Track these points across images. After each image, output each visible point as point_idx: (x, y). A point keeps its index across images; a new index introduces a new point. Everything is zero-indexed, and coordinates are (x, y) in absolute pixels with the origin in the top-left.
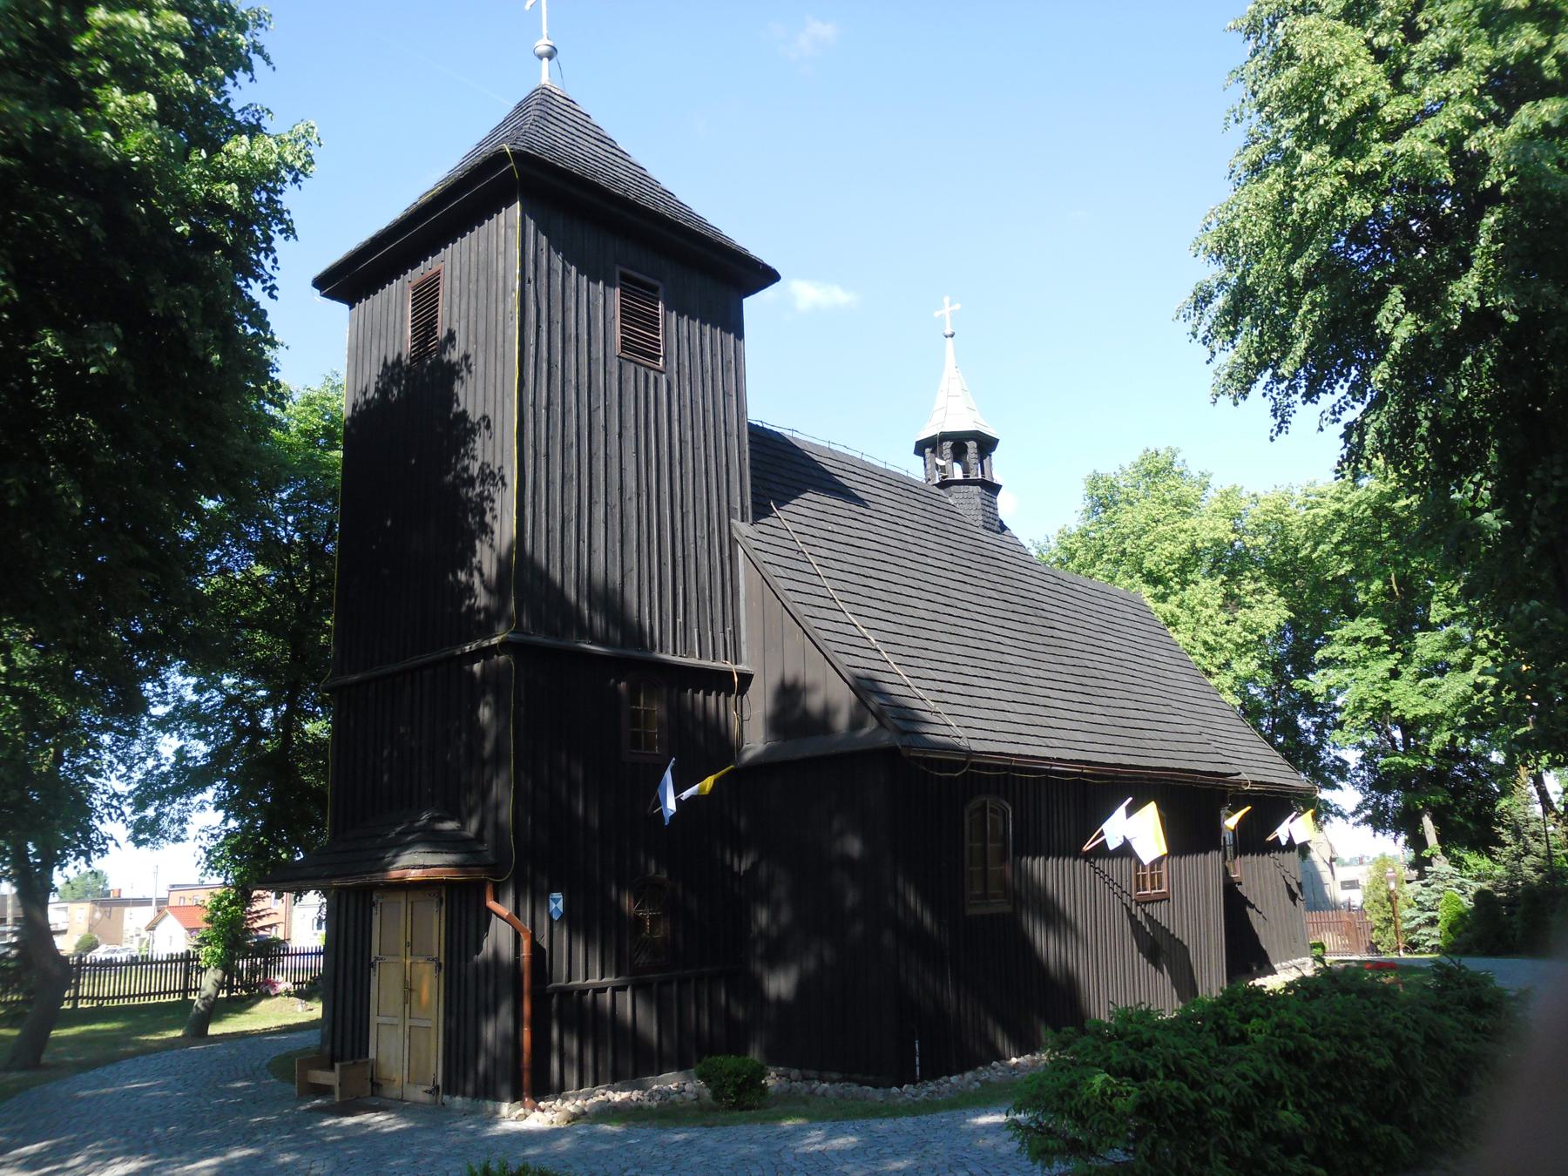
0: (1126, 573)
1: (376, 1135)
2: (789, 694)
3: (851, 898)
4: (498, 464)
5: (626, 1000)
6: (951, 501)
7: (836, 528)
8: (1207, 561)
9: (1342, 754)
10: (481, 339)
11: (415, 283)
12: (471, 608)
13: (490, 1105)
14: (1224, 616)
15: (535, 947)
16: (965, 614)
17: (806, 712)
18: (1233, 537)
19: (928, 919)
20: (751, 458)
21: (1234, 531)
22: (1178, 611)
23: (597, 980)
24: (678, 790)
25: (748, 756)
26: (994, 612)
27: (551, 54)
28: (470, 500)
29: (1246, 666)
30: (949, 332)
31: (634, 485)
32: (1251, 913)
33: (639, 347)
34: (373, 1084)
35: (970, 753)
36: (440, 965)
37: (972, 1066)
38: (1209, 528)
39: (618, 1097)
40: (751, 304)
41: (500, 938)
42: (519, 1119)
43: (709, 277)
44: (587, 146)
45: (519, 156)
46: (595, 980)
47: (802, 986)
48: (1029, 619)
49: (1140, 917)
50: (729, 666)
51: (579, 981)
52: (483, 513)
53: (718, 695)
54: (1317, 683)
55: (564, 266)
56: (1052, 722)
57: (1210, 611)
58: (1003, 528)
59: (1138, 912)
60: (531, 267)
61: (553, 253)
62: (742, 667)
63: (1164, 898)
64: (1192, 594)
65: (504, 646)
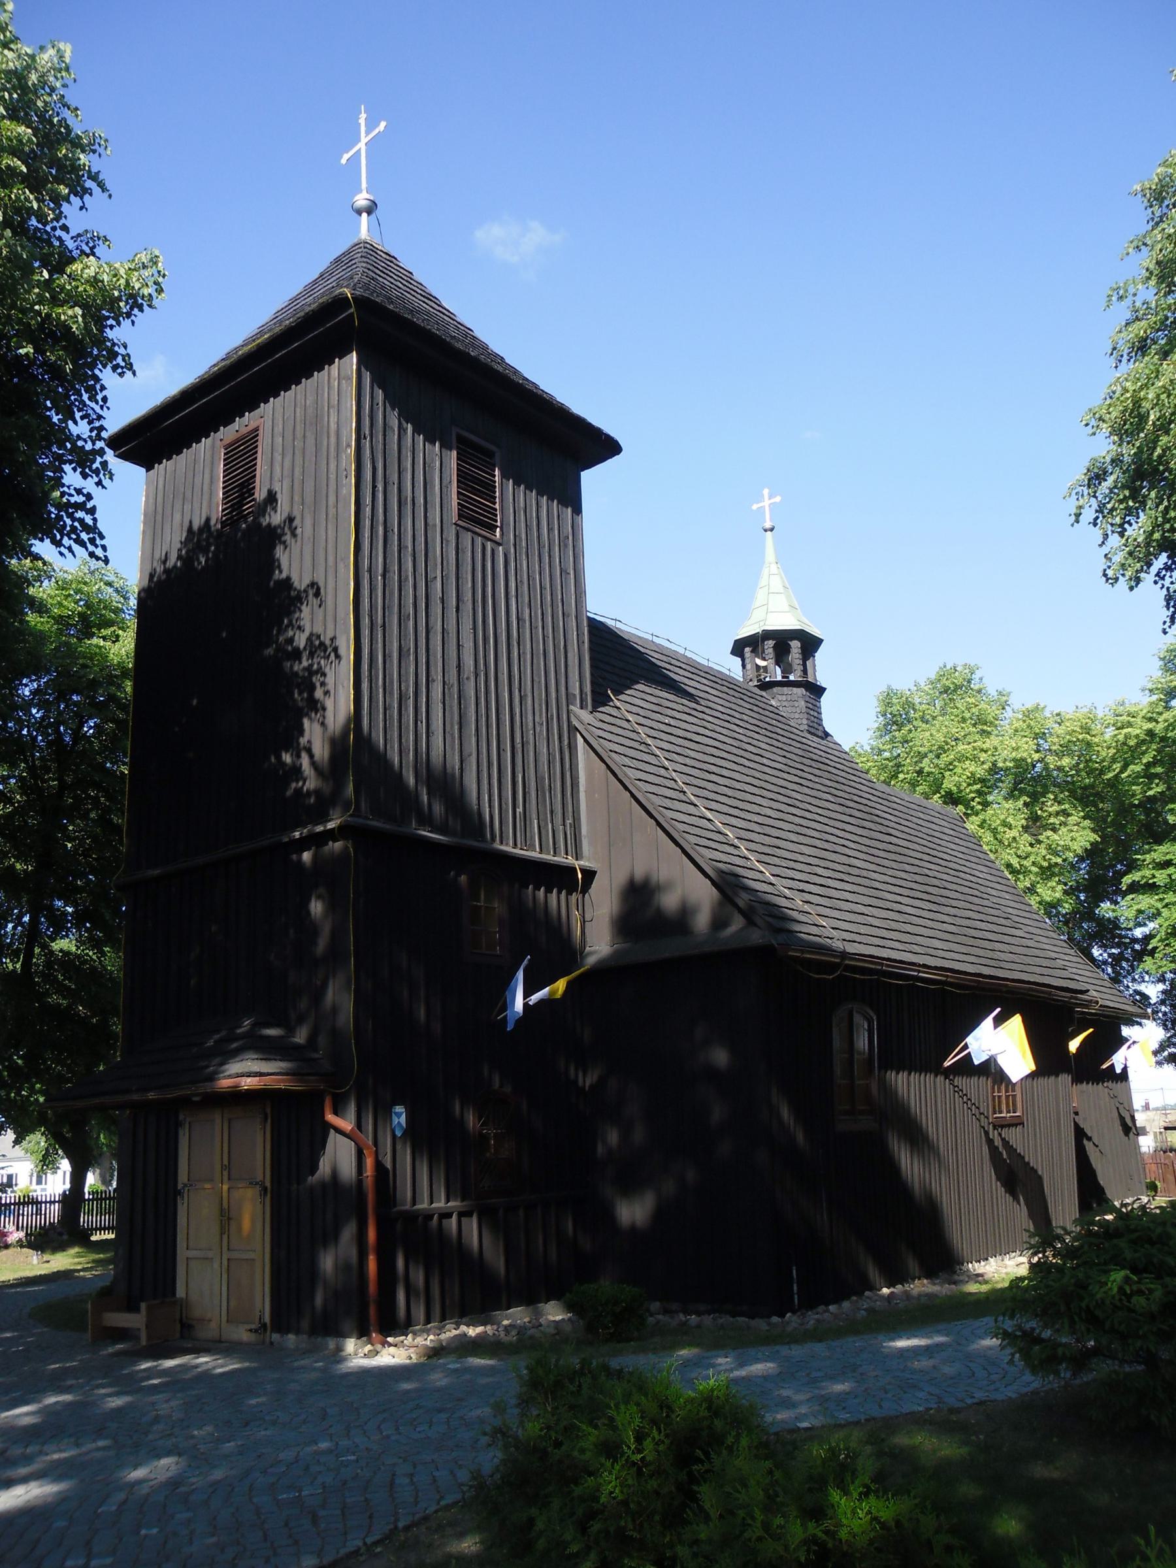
1: (206, 1377)
2: (639, 895)
3: (718, 1113)
4: (330, 634)
6: (773, 703)
7: (673, 722)
9: (1142, 988)
10: (309, 498)
12: (298, 791)
13: (331, 1344)
17: (659, 913)
19: (800, 1137)
20: (590, 641)
21: (1037, 751)
25: (591, 961)
27: (370, 210)
28: (296, 674)
29: (1051, 891)
30: (768, 525)
31: (472, 663)
33: (477, 515)
34: (183, 1325)
35: (844, 955)
36: (265, 1189)
37: (847, 1297)
38: (1010, 746)
39: (472, 1332)
40: (590, 479)
41: (340, 1156)
42: (360, 1354)
43: (553, 447)
44: (417, 302)
45: (360, 301)
46: (440, 1204)
47: (660, 1215)
49: (998, 1142)
50: (570, 860)
51: (423, 1205)
52: (312, 688)
53: (559, 893)
54: (1123, 910)
56: (909, 928)
57: (1014, 833)
58: (827, 734)
59: (994, 1135)
63: (1017, 1123)
65: (342, 832)
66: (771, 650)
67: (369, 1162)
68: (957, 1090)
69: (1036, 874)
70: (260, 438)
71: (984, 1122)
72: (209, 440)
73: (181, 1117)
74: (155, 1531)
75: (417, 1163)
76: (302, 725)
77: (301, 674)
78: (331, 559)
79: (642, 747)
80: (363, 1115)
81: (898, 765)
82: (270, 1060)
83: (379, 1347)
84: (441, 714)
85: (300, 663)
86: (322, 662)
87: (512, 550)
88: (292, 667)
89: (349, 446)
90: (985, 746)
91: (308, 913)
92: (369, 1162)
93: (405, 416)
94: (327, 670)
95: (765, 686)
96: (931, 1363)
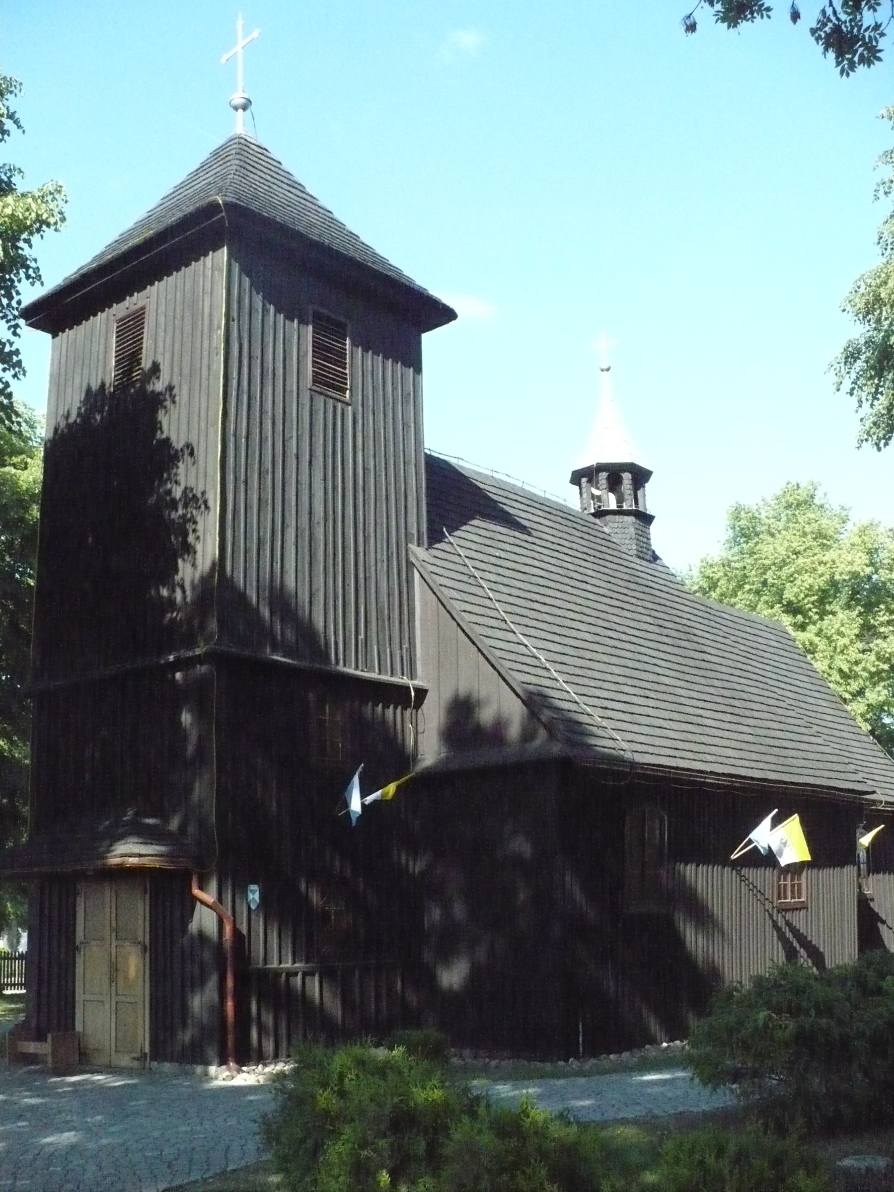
0: (767, 602)
2: (462, 709)
4: (201, 488)
5: (314, 986)
6: (606, 530)
7: (503, 554)
8: (845, 593)
10: (186, 371)
11: (120, 315)
13: (199, 1069)
14: (860, 645)
15: (236, 932)
16: (624, 637)
18: (868, 570)
22: (816, 640)
23: (289, 965)
24: (363, 795)
26: (650, 636)
31: (322, 509)
32: (883, 928)
33: (329, 381)
35: (633, 764)
36: (145, 947)
38: (848, 561)
40: (431, 341)
41: (204, 920)
44: (282, 193)
46: (288, 965)
47: (475, 977)
48: (683, 644)
49: (781, 923)
50: (405, 680)
51: (274, 965)
53: (395, 708)
55: (264, 305)
57: (846, 641)
58: (655, 558)
60: (235, 306)
61: (254, 293)
62: (418, 683)
63: (803, 907)
64: (830, 624)
66: (604, 482)
67: (228, 929)
68: (743, 879)
69: (867, 679)
70: (146, 316)
71: (768, 906)
72: (104, 315)
73: (78, 887)
74: (59, 1169)
75: (269, 931)
76: (177, 563)
77: (177, 521)
78: (203, 425)
79: (471, 580)
80: (224, 888)
81: (745, 576)
82: (147, 844)
83: (235, 1073)
84: (293, 555)
85: (177, 511)
86: (194, 511)
87: (360, 409)
88: (169, 515)
89: (219, 327)
90: (824, 559)
91: (180, 723)
92: (228, 929)
93: (268, 298)
94: (198, 519)
95: (600, 514)
96: (661, 1089)
